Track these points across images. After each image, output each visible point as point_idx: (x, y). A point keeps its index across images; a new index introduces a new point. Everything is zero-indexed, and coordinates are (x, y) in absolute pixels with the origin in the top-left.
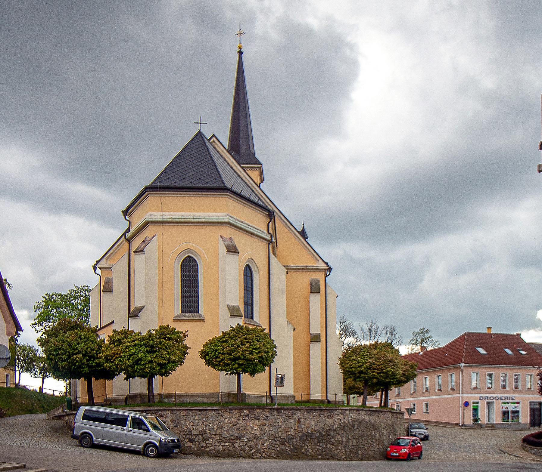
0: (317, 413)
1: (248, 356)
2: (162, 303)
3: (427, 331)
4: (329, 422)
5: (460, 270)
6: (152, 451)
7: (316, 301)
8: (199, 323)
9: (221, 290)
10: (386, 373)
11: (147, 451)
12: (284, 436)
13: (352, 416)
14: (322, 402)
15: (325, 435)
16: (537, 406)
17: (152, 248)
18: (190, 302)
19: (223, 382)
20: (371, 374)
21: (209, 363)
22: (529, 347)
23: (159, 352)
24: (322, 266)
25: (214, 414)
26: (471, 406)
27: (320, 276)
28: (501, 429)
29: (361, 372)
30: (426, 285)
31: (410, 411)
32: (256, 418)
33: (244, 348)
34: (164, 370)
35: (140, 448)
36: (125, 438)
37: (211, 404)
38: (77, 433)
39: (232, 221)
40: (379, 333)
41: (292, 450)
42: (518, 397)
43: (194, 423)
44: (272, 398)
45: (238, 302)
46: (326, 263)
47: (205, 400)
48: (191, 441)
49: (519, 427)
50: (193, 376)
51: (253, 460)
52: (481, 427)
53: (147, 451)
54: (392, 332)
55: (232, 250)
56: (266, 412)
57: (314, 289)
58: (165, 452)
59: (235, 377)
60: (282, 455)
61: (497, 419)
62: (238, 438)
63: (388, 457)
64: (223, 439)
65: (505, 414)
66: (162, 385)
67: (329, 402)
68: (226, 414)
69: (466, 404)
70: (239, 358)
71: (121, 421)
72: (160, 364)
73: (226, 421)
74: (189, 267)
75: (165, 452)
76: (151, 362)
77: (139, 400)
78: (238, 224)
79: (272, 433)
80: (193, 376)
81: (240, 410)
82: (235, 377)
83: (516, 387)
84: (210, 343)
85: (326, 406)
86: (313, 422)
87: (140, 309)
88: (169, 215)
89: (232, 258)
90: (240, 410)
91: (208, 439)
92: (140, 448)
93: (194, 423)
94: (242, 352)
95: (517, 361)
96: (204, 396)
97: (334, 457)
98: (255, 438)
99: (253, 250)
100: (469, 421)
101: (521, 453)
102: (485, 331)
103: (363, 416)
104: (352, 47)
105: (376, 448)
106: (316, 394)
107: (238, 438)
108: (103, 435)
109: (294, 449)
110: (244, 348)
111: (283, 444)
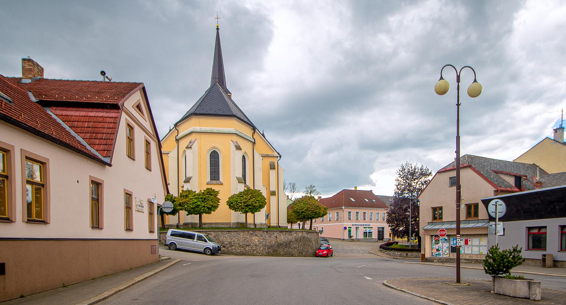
0: (285, 233)
1: (255, 204)
2: (200, 175)
3: (314, 187)
4: (290, 237)
5: (330, 150)
6: (208, 252)
7: (273, 173)
8: (220, 186)
9: (231, 168)
10: (316, 213)
11: (206, 251)
12: (269, 245)
13: (300, 234)
14: (276, 227)
15: (288, 244)
16: (381, 230)
17: (195, 146)
18: (215, 174)
19: (236, 217)
20: (308, 213)
21: (230, 207)
22: (376, 197)
23: (206, 202)
24: (276, 155)
25: (235, 233)
26: (348, 229)
27: (275, 160)
28: (363, 241)
29: (303, 212)
30: (309, 158)
31: (321, 232)
32: (256, 236)
33: (252, 200)
34: (209, 210)
35: (202, 250)
36: (194, 245)
37: (226, 228)
38: (168, 243)
39: (237, 133)
40: (286, 187)
41: (273, 252)
42: (372, 225)
43: (226, 238)
44: (255, 225)
45: (240, 176)
46: (278, 153)
47: (224, 226)
48: (224, 247)
49: (372, 241)
50: (223, 214)
51: (246, 257)
52: (353, 240)
53: (206, 251)
54: (293, 187)
55: (238, 148)
56: (261, 232)
57: (272, 167)
58: (214, 252)
59: (244, 215)
60: (269, 254)
61: (361, 236)
62: (247, 246)
63: (316, 255)
64: (240, 246)
65: (365, 233)
66: (207, 218)
67: (280, 227)
68: (242, 234)
69: (345, 228)
70: (250, 205)
71: (191, 237)
72: (208, 208)
73: (240, 237)
74: (214, 157)
75: (214, 252)
76: (204, 207)
77: (190, 226)
78: (240, 134)
79: (264, 243)
80: (223, 214)
81: (248, 231)
82: (244, 215)
83: (365, 219)
84: (232, 197)
85: (280, 229)
86: (283, 238)
87: (190, 178)
88: (204, 129)
89: (238, 151)
90: (248, 231)
91: (232, 246)
92: (202, 250)
93: (226, 238)
94: (249, 202)
95: (371, 205)
96: (223, 224)
97: (292, 256)
98: (256, 245)
99: (246, 147)
100: (346, 237)
101: (380, 253)
102: (354, 189)
103: (305, 234)
104: (270, 22)
105: (311, 251)
106: (274, 223)
107: (247, 246)
108: (182, 244)
109: (274, 251)
110: (252, 200)
111: (269, 248)
